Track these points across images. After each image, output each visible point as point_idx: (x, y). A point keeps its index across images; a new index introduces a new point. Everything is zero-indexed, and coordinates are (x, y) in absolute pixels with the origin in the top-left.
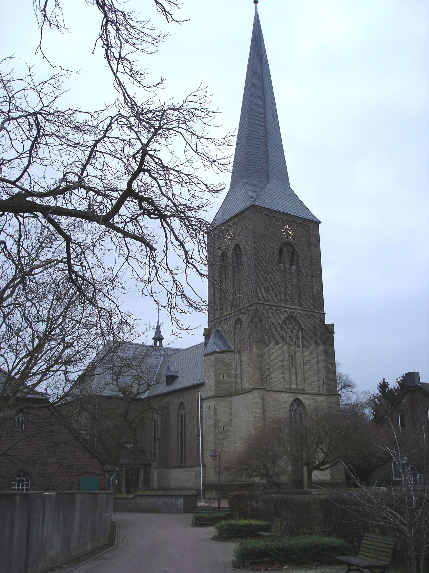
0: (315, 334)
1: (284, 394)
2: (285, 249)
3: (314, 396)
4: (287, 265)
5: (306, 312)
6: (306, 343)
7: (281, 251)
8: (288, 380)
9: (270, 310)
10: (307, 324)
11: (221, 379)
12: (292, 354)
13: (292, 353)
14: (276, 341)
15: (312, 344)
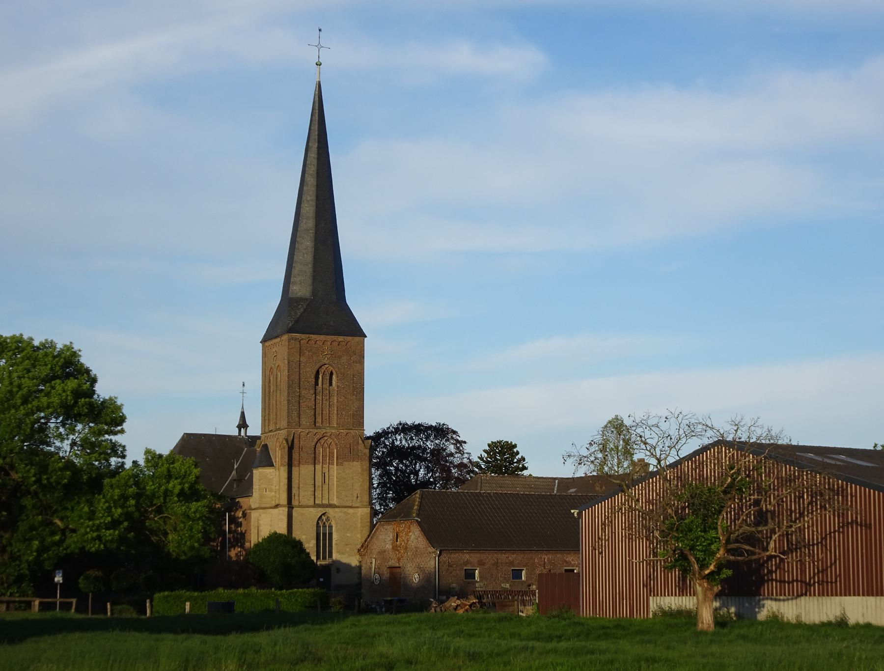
3: (346, 510)
10: (343, 442)
11: (265, 493)
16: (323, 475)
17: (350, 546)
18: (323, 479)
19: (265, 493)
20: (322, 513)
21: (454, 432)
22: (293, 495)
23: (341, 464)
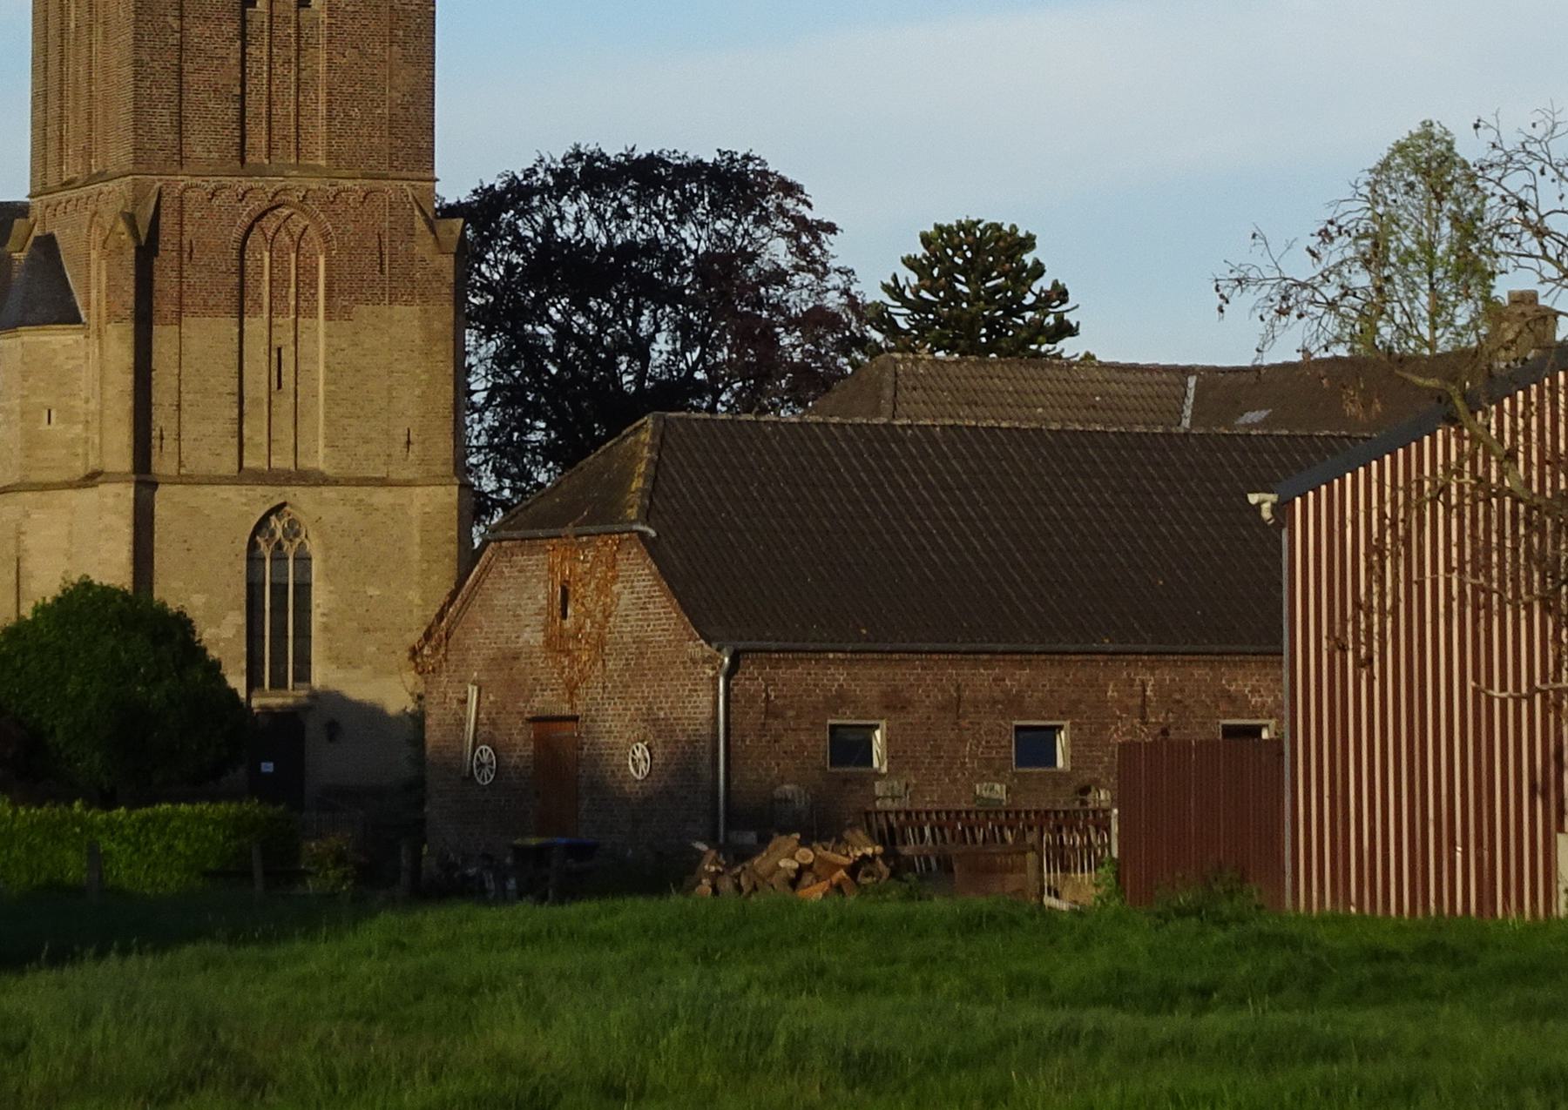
3: (362, 492)
6: (340, 301)
10: (351, 227)
11: (44, 426)
14: (211, 303)
16: (275, 355)
17: (379, 635)
18: (275, 373)
19: (44, 426)
20: (267, 507)
21: (790, 189)
22: (155, 433)
23: (346, 314)
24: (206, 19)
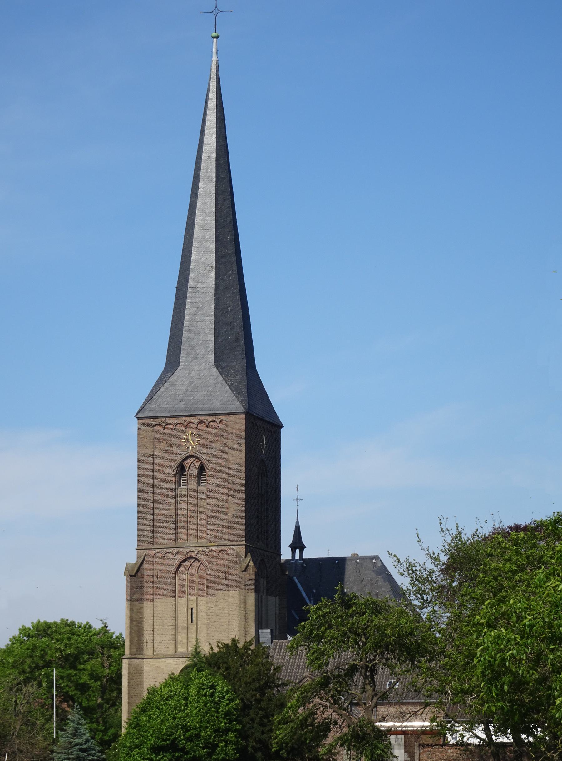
0: (227, 574)
1: (171, 661)
2: (187, 464)
4: (192, 486)
5: (213, 548)
7: (181, 469)
8: (185, 641)
9: (157, 555)
10: (215, 563)
12: (192, 606)
13: (194, 605)
14: (165, 593)
15: (221, 590)
16: (190, 611)
22: (145, 641)
24: (163, 492)
